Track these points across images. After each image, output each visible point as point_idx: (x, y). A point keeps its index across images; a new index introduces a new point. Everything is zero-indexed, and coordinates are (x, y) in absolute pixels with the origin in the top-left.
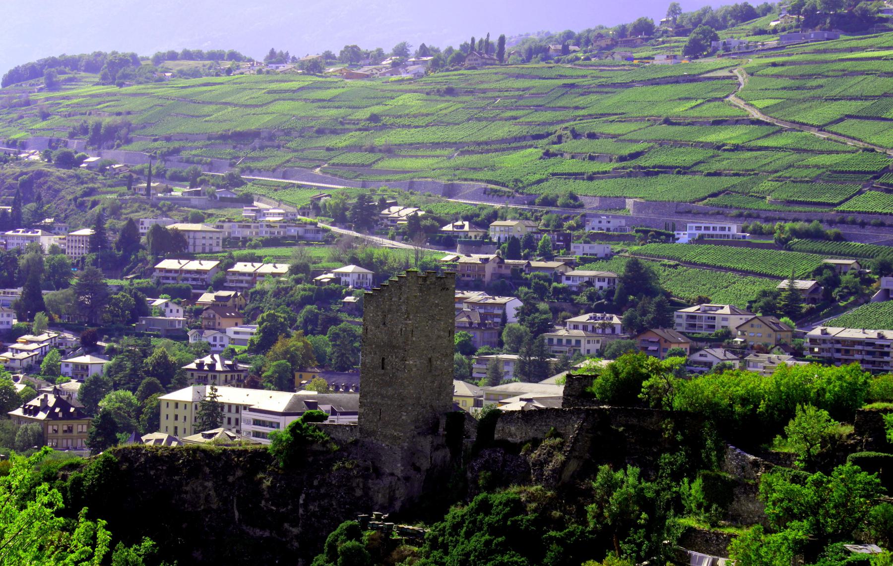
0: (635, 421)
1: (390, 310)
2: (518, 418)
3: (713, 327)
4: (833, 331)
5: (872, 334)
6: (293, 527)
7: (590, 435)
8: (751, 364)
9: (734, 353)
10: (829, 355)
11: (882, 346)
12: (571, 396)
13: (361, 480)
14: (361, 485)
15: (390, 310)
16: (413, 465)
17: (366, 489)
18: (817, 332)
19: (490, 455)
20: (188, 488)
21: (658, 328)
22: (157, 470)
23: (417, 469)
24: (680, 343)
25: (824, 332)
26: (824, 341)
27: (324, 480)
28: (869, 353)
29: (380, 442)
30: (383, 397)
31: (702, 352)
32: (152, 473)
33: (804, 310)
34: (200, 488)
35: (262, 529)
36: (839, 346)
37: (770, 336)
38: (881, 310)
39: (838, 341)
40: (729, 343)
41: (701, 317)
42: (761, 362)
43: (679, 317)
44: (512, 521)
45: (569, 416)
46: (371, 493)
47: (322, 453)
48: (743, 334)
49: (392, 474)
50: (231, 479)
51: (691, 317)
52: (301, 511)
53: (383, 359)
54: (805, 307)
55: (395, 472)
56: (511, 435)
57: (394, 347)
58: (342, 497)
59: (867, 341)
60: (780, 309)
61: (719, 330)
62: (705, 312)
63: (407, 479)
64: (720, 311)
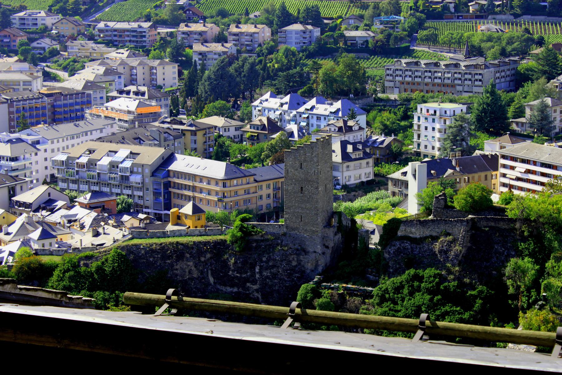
0: (493, 224)
1: (305, 161)
2: (417, 224)
3: (36, 24)
4: (111, 24)
5: (135, 25)
6: (253, 285)
7: (469, 234)
8: (70, 47)
9: (55, 40)
10: (110, 38)
11: (141, 32)
12: (439, 208)
13: (295, 256)
14: (295, 259)
15: (305, 161)
16: (324, 245)
17: (299, 262)
18: (101, 25)
19: (400, 245)
20: (178, 267)
21: (7, 28)
22: (154, 257)
23: (327, 247)
24: (22, 36)
25: (106, 26)
26: (107, 31)
27: (270, 257)
28: (133, 36)
29: (302, 234)
30: (302, 208)
31: (38, 42)
32: (151, 259)
33: (83, 10)
34: (185, 266)
35: (232, 286)
36: (116, 33)
37: (73, 29)
38: (125, 7)
39: (115, 30)
40: (49, 34)
41: (28, 19)
42: (76, 46)
43: (15, 19)
44: (443, 287)
45: (455, 223)
46: (302, 263)
47: (262, 241)
48: (56, 28)
49: (315, 252)
50: (203, 259)
51: (22, 19)
52: (257, 276)
53: (302, 188)
54: (83, 8)
55: (317, 251)
56: (412, 233)
57: (310, 181)
58: (284, 266)
59: (132, 29)
60: (69, 10)
61: (40, 26)
62: (30, 15)
63: (324, 253)
64: (39, 15)
